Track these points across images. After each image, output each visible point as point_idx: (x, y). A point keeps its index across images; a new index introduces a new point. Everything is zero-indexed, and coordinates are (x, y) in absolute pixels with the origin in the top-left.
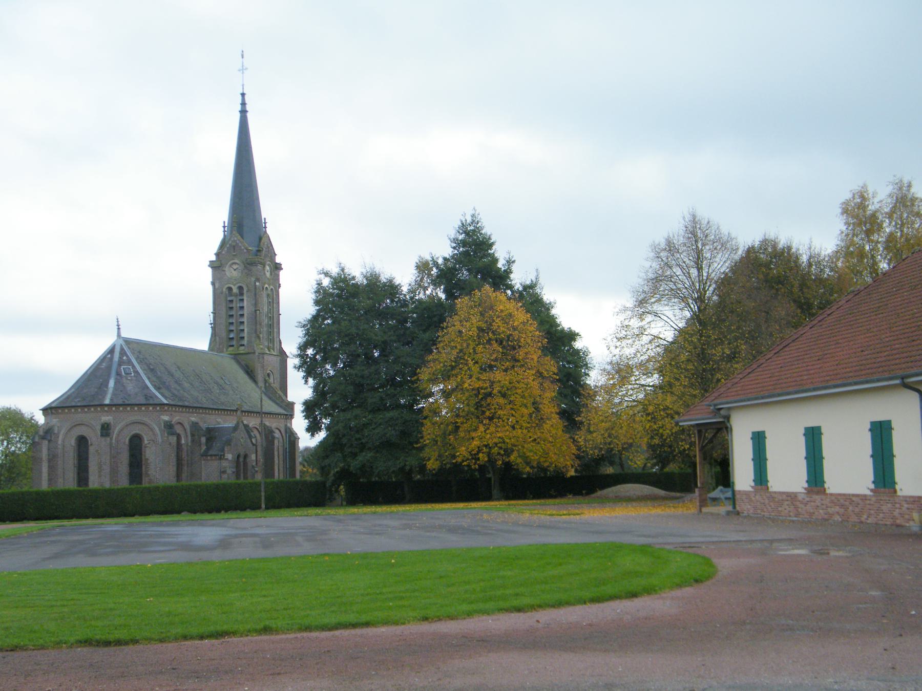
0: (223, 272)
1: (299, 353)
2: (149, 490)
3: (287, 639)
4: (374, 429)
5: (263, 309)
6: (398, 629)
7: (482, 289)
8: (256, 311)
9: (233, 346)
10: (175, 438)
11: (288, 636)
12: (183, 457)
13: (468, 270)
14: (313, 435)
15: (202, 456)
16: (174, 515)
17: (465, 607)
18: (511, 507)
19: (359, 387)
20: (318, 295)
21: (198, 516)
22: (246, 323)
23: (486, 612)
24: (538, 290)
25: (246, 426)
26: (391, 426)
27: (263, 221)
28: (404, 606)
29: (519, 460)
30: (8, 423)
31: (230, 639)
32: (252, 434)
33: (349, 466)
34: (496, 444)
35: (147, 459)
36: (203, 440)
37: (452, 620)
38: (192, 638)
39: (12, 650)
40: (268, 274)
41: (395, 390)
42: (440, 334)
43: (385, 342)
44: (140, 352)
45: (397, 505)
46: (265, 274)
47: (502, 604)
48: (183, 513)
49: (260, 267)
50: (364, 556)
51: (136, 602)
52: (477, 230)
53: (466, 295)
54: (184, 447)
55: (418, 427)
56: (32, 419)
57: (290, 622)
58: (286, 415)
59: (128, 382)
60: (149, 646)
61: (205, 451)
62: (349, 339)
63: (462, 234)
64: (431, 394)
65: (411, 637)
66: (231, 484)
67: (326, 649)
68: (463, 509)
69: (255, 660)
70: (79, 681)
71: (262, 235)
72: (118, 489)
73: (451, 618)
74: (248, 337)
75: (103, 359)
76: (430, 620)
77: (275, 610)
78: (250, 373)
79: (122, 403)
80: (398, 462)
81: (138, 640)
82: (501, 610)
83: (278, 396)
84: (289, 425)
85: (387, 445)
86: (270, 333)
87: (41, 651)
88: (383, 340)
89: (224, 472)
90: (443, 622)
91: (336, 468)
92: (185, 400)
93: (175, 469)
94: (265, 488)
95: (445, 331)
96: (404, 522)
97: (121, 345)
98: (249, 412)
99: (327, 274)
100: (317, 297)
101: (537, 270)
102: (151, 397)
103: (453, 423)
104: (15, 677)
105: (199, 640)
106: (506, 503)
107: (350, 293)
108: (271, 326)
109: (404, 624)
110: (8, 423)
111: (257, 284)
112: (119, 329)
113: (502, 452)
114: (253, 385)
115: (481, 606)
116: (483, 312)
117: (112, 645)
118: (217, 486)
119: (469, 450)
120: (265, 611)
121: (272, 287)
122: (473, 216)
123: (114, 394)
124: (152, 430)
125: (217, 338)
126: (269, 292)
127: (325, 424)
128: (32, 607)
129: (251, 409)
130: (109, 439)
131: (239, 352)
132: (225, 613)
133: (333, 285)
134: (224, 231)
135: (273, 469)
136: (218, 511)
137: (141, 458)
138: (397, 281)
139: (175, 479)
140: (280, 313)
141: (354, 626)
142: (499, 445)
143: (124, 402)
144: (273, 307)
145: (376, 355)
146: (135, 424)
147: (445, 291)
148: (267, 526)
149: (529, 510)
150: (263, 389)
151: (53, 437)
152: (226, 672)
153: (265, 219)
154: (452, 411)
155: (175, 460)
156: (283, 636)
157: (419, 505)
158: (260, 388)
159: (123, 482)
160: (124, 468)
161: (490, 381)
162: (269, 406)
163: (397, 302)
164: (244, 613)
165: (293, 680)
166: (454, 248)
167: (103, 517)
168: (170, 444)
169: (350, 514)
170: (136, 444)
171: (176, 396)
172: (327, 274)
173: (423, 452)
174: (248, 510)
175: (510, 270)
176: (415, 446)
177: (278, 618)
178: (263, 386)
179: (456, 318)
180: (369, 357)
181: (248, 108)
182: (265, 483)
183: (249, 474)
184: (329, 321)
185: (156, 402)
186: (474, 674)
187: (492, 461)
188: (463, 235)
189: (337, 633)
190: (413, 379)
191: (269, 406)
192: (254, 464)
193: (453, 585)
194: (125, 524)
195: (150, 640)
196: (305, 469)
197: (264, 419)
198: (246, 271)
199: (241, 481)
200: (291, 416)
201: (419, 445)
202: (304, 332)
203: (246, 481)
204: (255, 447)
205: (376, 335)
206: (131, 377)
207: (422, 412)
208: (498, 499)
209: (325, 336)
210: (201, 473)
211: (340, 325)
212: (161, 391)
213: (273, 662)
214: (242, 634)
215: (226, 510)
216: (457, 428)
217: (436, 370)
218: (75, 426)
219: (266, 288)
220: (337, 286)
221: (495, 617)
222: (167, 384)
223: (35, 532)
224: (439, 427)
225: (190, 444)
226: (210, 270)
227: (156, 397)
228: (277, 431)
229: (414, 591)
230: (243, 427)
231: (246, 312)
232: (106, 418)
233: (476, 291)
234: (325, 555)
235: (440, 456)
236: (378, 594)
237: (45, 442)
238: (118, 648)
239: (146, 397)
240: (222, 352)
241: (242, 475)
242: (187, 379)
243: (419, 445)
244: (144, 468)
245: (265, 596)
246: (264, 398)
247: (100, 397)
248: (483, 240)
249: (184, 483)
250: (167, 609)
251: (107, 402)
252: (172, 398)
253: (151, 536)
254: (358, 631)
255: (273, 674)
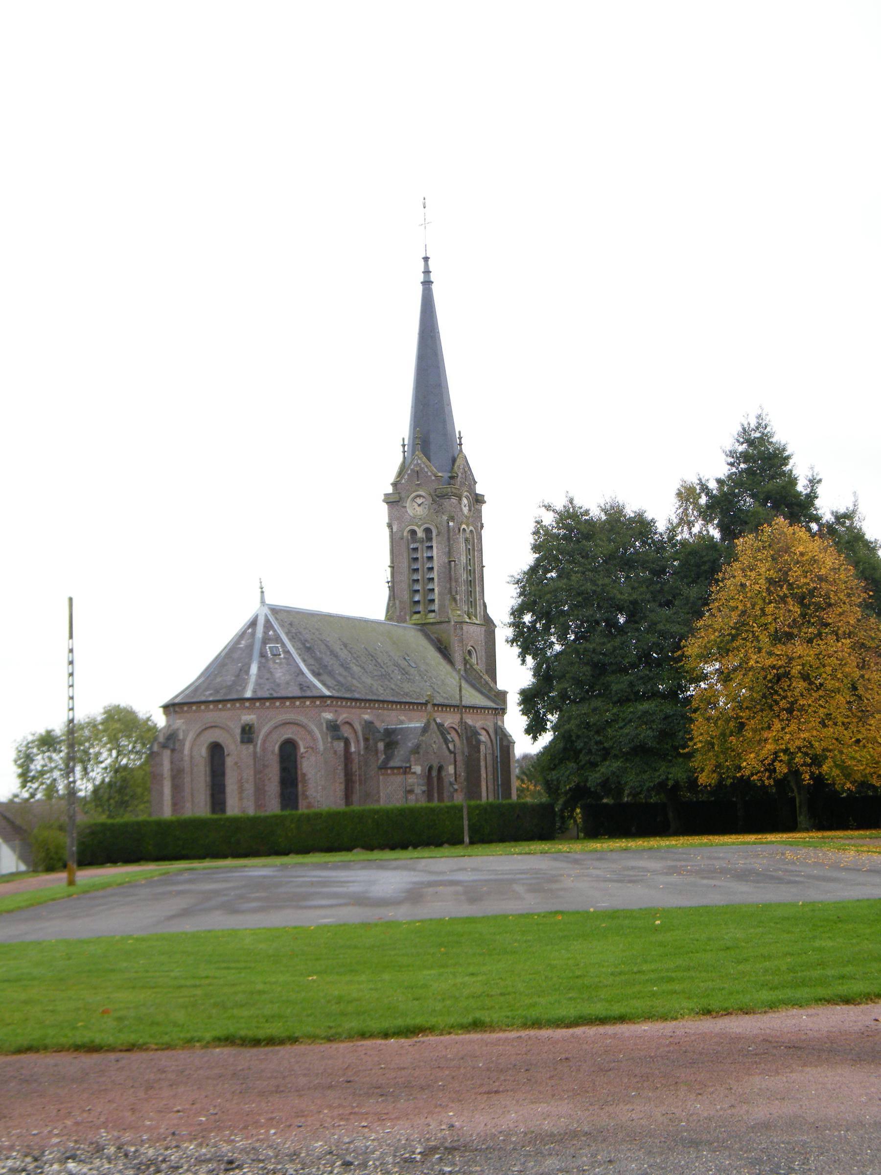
0: (403, 510)
1: (512, 620)
2: (308, 818)
3: (506, 1039)
4: (621, 728)
5: (459, 559)
6: (667, 1027)
7: (773, 523)
8: (450, 562)
9: (419, 612)
10: (342, 744)
11: (507, 1035)
12: (354, 770)
13: (752, 496)
14: (535, 738)
15: (380, 768)
16: (343, 853)
17: (765, 995)
18: (827, 840)
19: (600, 669)
20: (536, 537)
21: (377, 855)
22: (436, 580)
23: (798, 1004)
24: (857, 524)
25: (440, 726)
26: (646, 724)
27: (458, 436)
28: (675, 992)
29: (836, 772)
30: (117, 725)
31: (425, 1039)
32: (449, 737)
33: (586, 780)
34: (799, 748)
35: (304, 775)
36: (381, 746)
37: (747, 1014)
38: (372, 1036)
39: (128, 1050)
40: (466, 510)
41: (650, 671)
42: (713, 589)
43: (634, 603)
44: (291, 624)
45: (658, 838)
46: (461, 510)
47: (821, 992)
48: (355, 851)
49: (454, 500)
50: (613, 915)
51: (294, 981)
52: (764, 439)
53: (751, 532)
54: (355, 758)
55: (685, 724)
56: (148, 719)
57: (509, 1014)
58: (496, 709)
59: (276, 666)
60: (312, 1046)
61: (383, 762)
62: (583, 599)
63: (742, 443)
64: (705, 677)
65: (688, 1039)
66: (422, 808)
67: (563, 1056)
68: (755, 843)
69: (462, 1071)
70: (219, 1097)
71: (456, 456)
72: (267, 818)
73: (746, 1011)
74: (439, 600)
75: (242, 635)
76: (714, 1014)
77: (488, 995)
78: (444, 651)
79: (268, 696)
80: (657, 774)
81: (297, 1038)
82: (820, 1000)
83: (483, 682)
84: (499, 723)
85: (640, 751)
86: (470, 593)
87: (166, 1052)
88: (631, 599)
89: (411, 791)
90: (733, 1016)
91: (569, 784)
92: (355, 691)
93: (343, 787)
94: (468, 813)
95: (721, 584)
96: (670, 863)
97: (266, 616)
98: (444, 706)
99: (548, 508)
100: (536, 540)
101: (855, 493)
102: (308, 687)
103: (735, 719)
104: (132, 1090)
105: (382, 1039)
106: (819, 834)
107: (582, 534)
108: (471, 583)
109: (676, 1019)
110: (117, 725)
111: (451, 524)
112: (262, 592)
113: (809, 761)
114: (448, 667)
115: (789, 993)
116: (776, 556)
117: (263, 1044)
118: (403, 813)
119: (761, 758)
120: (473, 997)
121: (471, 528)
122: (759, 417)
123: (258, 684)
124: (310, 732)
125: (397, 602)
126: (468, 536)
127: (552, 722)
128: (154, 988)
129: (446, 702)
130: (251, 746)
131: (428, 621)
132: (417, 999)
133: (557, 523)
134: (404, 452)
135: (479, 785)
136: (404, 847)
137: (296, 773)
138: (649, 516)
139: (343, 802)
140: (484, 564)
141: (602, 1021)
142: (804, 750)
143: (271, 694)
144: (474, 557)
145: (622, 620)
146: (291, 726)
147: (722, 527)
148: (473, 870)
149: (853, 845)
150: (462, 672)
151: (177, 745)
152: (422, 1088)
153: (460, 433)
154: (734, 700)
155: (342, 775)
156: (501, 1035)
157: (690, 838)
158: (458, 671)
159: (273, 807)
160: (273, 787)
161: (787, 656)
162: (472, 697)
163: (649, 545)
164: (443, 1000)
165: (517, 1101)
166: (732, 464)
167: (246, 855)
168: (335, 752)
169: (591, 851)
170: (289, 751)
171: (342, 685)
172: (548, 508)
173: (693, 759)
174: (446, 845)
175: (815, 493)
176: (681, 751)
177: (492, 1007)
178: (463, 668)
179: (736, 565)
180: (612, 623)
181: (433, 277)
182: (469, 807)
183: (446, 794)
184: (553, 574)
185: (315, 693)
186: (784, 1099)
187: (795, 773)
188: (745, 445)
189: (579, 1031)
190: (676, 655)
191: (472, 697)
192: (452, 779)
193: (746, 960)
194: (276, 866)
195: (313, 1038)
196: (524, 786)
197: (464, 716)
198: (435, 506)
199: (435, 804)
200: (503, 711)
201: (687, 750)
202: (518, 590)
203: (442, 805)
204: (452, 755)
205: (621, 593)
206: (280, 659)
207: (690, 702)
208: (807, 830)
209: (549, 596)
210: (378, 793)
211: (569, 579)
212: (322, 678)
213: (488, 1073)
214: (442, 1030)
215: (415, 846)
216: (742, 725)
217: (709, 642)
218: (206, 729)
219: (464, 529)
220: (563, 524)
221: (811, 1011)
222: (330, 668)
223: (156, 878)
224: (715, 723)
225: (362, 753)
226: (385, 507)
227: (315, 686)
228: (483, 732)
229: (688, 969)
230: (435, 727)
231: (435, 564)
232: (248, 718)
233: (765, 525)
234: (557, 913)
235: (718, 766)
236: (636, 973)
237: (167, 753)
238: (270, 1049)
239: (301, 687)
240: (405, 621)
241: (436, 795)
242: (357, 661)
243: (687, 750)
244: (300, 786)
245: (473, 974)
246: (464, 685)
247: (240, 688)
248: (775, 451)
249: (356, 807)
250: (336, 993)
251: (248, 694)
252: (336, 688)
253: (312, 884)
254: (609, 1029)
255: (489, 1093)
